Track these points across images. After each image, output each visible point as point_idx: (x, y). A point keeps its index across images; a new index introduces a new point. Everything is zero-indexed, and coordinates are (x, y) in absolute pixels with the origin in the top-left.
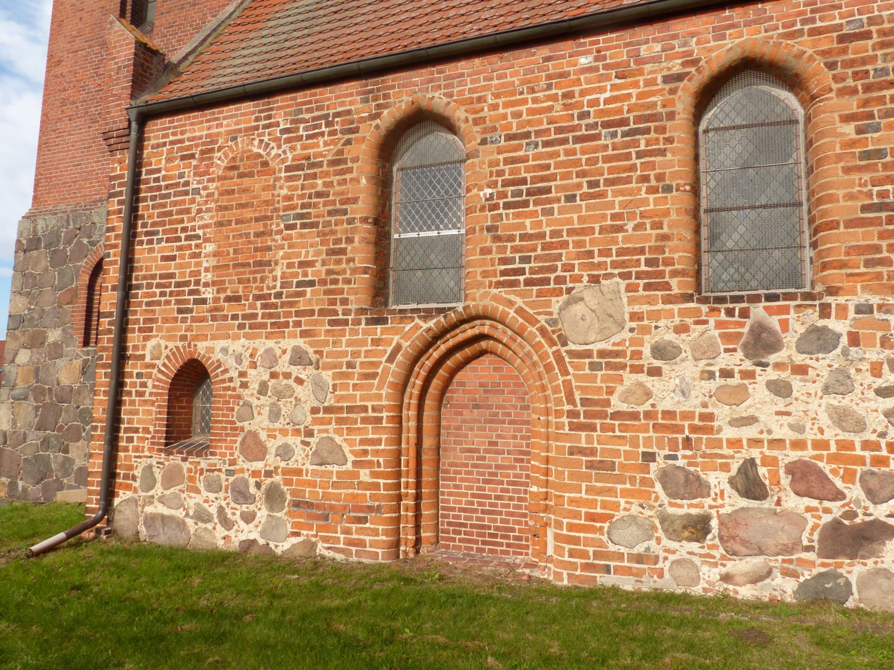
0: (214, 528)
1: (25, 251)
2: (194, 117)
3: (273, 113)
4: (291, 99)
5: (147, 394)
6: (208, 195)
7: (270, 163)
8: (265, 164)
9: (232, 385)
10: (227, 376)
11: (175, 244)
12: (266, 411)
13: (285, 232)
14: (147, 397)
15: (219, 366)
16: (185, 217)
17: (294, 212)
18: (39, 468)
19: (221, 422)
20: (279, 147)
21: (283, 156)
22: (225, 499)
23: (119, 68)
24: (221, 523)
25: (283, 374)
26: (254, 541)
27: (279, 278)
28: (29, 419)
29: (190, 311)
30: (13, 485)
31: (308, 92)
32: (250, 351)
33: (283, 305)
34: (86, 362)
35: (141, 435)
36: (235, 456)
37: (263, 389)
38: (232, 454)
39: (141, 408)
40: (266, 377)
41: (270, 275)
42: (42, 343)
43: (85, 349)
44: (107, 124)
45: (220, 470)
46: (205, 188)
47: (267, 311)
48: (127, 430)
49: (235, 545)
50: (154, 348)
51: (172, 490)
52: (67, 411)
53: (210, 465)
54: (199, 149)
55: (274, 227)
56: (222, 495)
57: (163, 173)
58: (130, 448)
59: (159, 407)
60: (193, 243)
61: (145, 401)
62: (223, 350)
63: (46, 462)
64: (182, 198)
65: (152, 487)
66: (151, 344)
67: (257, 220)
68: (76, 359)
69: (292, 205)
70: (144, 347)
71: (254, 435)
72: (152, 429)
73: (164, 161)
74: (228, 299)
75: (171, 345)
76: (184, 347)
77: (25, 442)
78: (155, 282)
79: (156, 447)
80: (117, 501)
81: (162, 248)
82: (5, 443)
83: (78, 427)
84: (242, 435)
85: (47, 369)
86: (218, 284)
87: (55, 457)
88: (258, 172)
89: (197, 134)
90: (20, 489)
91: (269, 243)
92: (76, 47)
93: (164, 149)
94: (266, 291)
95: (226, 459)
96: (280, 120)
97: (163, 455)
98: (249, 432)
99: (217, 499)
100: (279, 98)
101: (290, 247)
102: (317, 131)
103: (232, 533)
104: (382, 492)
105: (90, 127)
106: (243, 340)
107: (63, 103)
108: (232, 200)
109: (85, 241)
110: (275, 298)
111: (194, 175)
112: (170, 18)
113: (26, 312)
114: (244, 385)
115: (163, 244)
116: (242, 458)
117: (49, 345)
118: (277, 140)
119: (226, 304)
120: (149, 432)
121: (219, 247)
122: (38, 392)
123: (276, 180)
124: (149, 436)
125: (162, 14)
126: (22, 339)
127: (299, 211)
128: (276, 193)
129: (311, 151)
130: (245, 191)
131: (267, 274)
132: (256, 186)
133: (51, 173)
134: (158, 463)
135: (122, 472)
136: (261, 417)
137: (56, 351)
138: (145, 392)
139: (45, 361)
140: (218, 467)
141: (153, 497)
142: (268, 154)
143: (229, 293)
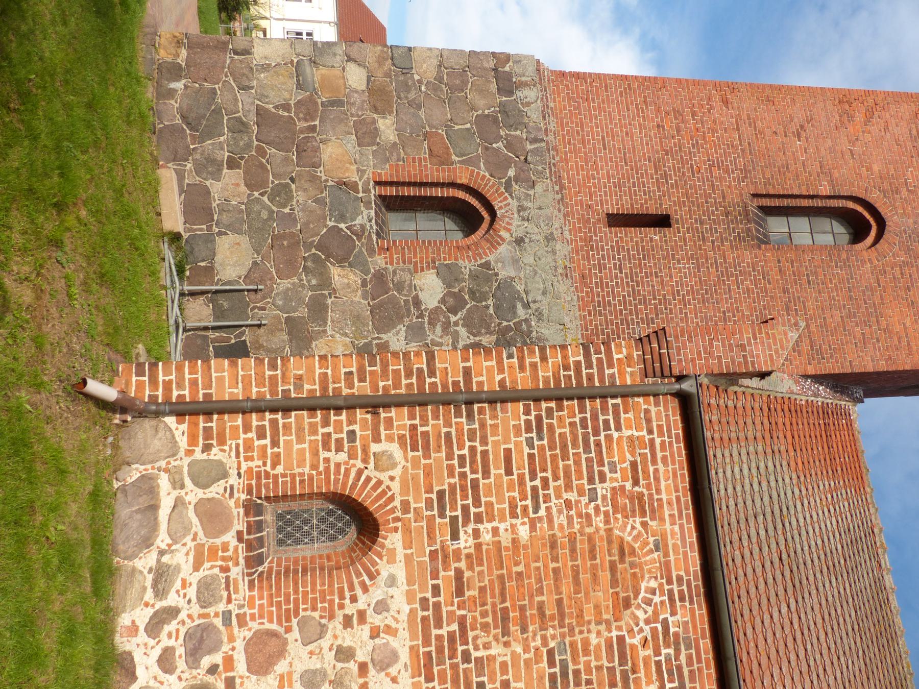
0: (147, 605)
1: (495, 70)
2: (682, 475)
3: (687, 604)
4: (703, 630)
5: (327, 455)
6: (588, 516)
7: (628, 612)
8: (627, 604)
9: (347, 601)
10: (359, 591)
11: (527, 471)
12: (315, 664)
13: (545, 650)
14: (323, 454)
15: (372, 577)
16: (561, 482)
17: (569, 660)
18: (203, 117)
19: (296, 592)
20: (647, 622)
21: (636, 629)
22: (190, 616)
23: (743, 347)
24: (156, 614)
25: (366, 683)
26: (133, 677)
27: (488, 652)
28: (272, 94)
29: (442, 515)
30: (175, 71)
31: (711, 656)
32: (394, 625)
33: (454, 667)
34: (354, 187)
35: (269, 451)
36: (251, 624)
37: (344, 654)
38: (253, 617)
39: (306, 446)
40: (361, 656)
41: (491, 638)
42: (375, 109)
43: (372, 183)
44: (676, 337)
45: (229, 601)
46: (597, 509)
47: (446, 643)
48: (274, 422)
49: (123, 643)
50: (391, 457)
51: (195, 520)
52: (287, 160)
53: (236, 580)
54: (645, 491)
55: (551, 631)
56: (196, 609)
57: (616, 435)
58: (249, 435)
59: (311, 478)
60: (529, 502)
61: (316, 454)
62: (393, 579)
63: (211, 132)
64: (585, 473)
65: (196, 484)
66: (394, 449)
67: (559, 602)
68: (358, 170)
69: (578, 654)
70: (390, 439)
71: (281, 652)
72: (280, 469)
73: (629, 433)
74: (459, 574)
75: (396, 486)
76: (393, 510)
77: (239, 89)
78: (477, 444)
79: (254, 482)
80: (171, 420)
81: (520, 446)
82: (236, 53)
83: (264, 184)
84: (281, 630)
85: (341, 121)
86: (476, 557)
87: (220, 145)
88: (617, 593)
89: (663, 484)
90: (173, 85)
91: (531, 628)
92: (743, 128)
93: (645, 433)
94: (471, 634)
95: (246, 609)
96: (678, 617)
97: (243, 497)
98: (285, 642)
99: (189, 601)
100: (704, 611)
101: (527, 662)
102: (666, 676)
103: (142, 637)
104: (201, 392)
105: (650, 161)
106: (406, 609)
107: (678, 113)
108: (583, 559)
109: (511, 173)
110: (463, 652)
111: (614, 489)
112: (774, 274)
113: (416, 77)
114: (347, 622)
115: (526, 450)
116: (249, 634)
117: (374, 122)
118: (655, 617)
119: (452, 573)
120: (274, 467)
121: (525, 547)
122: (308, 107)
123: (608, 622)
124: (268, 468)
125: (779, 261)
126: (379, 74)
127: (571, 667)
128: (593, 627)
129: (642, 674)
130: (595, 577)
131: (493, 632)
132: (601, 594)
133: (594, 101)
134: (232, 487)
135: (214, 425)
136: (305, 656)
137: (367, 134)
138: (329, 450)
139: (352, 115)
140: (233, 596)
141: (182, 487)
142: (639, 607)
143: (467, 574)
